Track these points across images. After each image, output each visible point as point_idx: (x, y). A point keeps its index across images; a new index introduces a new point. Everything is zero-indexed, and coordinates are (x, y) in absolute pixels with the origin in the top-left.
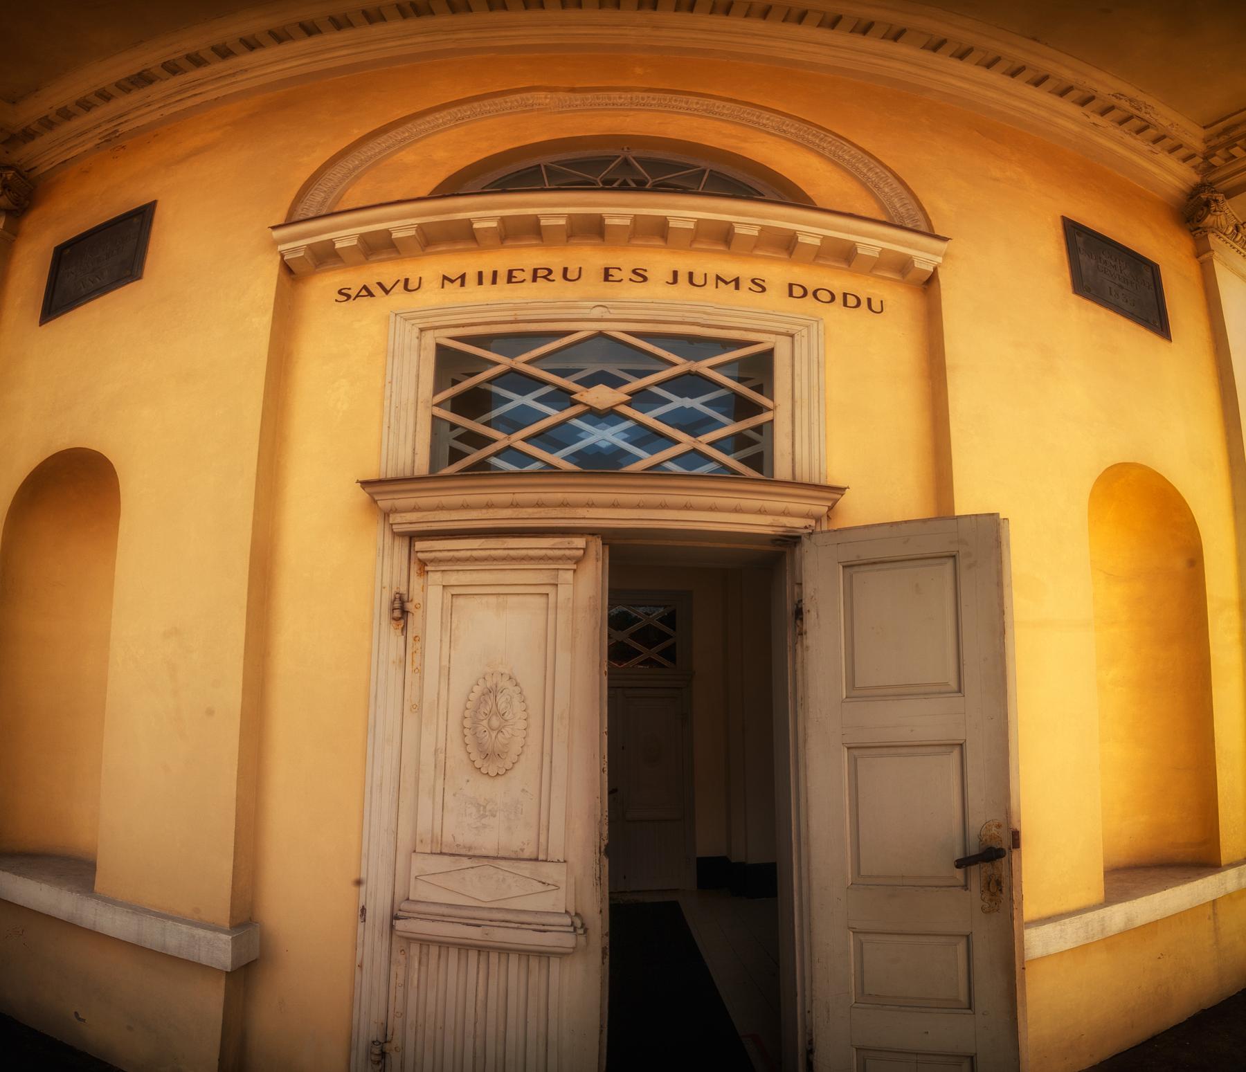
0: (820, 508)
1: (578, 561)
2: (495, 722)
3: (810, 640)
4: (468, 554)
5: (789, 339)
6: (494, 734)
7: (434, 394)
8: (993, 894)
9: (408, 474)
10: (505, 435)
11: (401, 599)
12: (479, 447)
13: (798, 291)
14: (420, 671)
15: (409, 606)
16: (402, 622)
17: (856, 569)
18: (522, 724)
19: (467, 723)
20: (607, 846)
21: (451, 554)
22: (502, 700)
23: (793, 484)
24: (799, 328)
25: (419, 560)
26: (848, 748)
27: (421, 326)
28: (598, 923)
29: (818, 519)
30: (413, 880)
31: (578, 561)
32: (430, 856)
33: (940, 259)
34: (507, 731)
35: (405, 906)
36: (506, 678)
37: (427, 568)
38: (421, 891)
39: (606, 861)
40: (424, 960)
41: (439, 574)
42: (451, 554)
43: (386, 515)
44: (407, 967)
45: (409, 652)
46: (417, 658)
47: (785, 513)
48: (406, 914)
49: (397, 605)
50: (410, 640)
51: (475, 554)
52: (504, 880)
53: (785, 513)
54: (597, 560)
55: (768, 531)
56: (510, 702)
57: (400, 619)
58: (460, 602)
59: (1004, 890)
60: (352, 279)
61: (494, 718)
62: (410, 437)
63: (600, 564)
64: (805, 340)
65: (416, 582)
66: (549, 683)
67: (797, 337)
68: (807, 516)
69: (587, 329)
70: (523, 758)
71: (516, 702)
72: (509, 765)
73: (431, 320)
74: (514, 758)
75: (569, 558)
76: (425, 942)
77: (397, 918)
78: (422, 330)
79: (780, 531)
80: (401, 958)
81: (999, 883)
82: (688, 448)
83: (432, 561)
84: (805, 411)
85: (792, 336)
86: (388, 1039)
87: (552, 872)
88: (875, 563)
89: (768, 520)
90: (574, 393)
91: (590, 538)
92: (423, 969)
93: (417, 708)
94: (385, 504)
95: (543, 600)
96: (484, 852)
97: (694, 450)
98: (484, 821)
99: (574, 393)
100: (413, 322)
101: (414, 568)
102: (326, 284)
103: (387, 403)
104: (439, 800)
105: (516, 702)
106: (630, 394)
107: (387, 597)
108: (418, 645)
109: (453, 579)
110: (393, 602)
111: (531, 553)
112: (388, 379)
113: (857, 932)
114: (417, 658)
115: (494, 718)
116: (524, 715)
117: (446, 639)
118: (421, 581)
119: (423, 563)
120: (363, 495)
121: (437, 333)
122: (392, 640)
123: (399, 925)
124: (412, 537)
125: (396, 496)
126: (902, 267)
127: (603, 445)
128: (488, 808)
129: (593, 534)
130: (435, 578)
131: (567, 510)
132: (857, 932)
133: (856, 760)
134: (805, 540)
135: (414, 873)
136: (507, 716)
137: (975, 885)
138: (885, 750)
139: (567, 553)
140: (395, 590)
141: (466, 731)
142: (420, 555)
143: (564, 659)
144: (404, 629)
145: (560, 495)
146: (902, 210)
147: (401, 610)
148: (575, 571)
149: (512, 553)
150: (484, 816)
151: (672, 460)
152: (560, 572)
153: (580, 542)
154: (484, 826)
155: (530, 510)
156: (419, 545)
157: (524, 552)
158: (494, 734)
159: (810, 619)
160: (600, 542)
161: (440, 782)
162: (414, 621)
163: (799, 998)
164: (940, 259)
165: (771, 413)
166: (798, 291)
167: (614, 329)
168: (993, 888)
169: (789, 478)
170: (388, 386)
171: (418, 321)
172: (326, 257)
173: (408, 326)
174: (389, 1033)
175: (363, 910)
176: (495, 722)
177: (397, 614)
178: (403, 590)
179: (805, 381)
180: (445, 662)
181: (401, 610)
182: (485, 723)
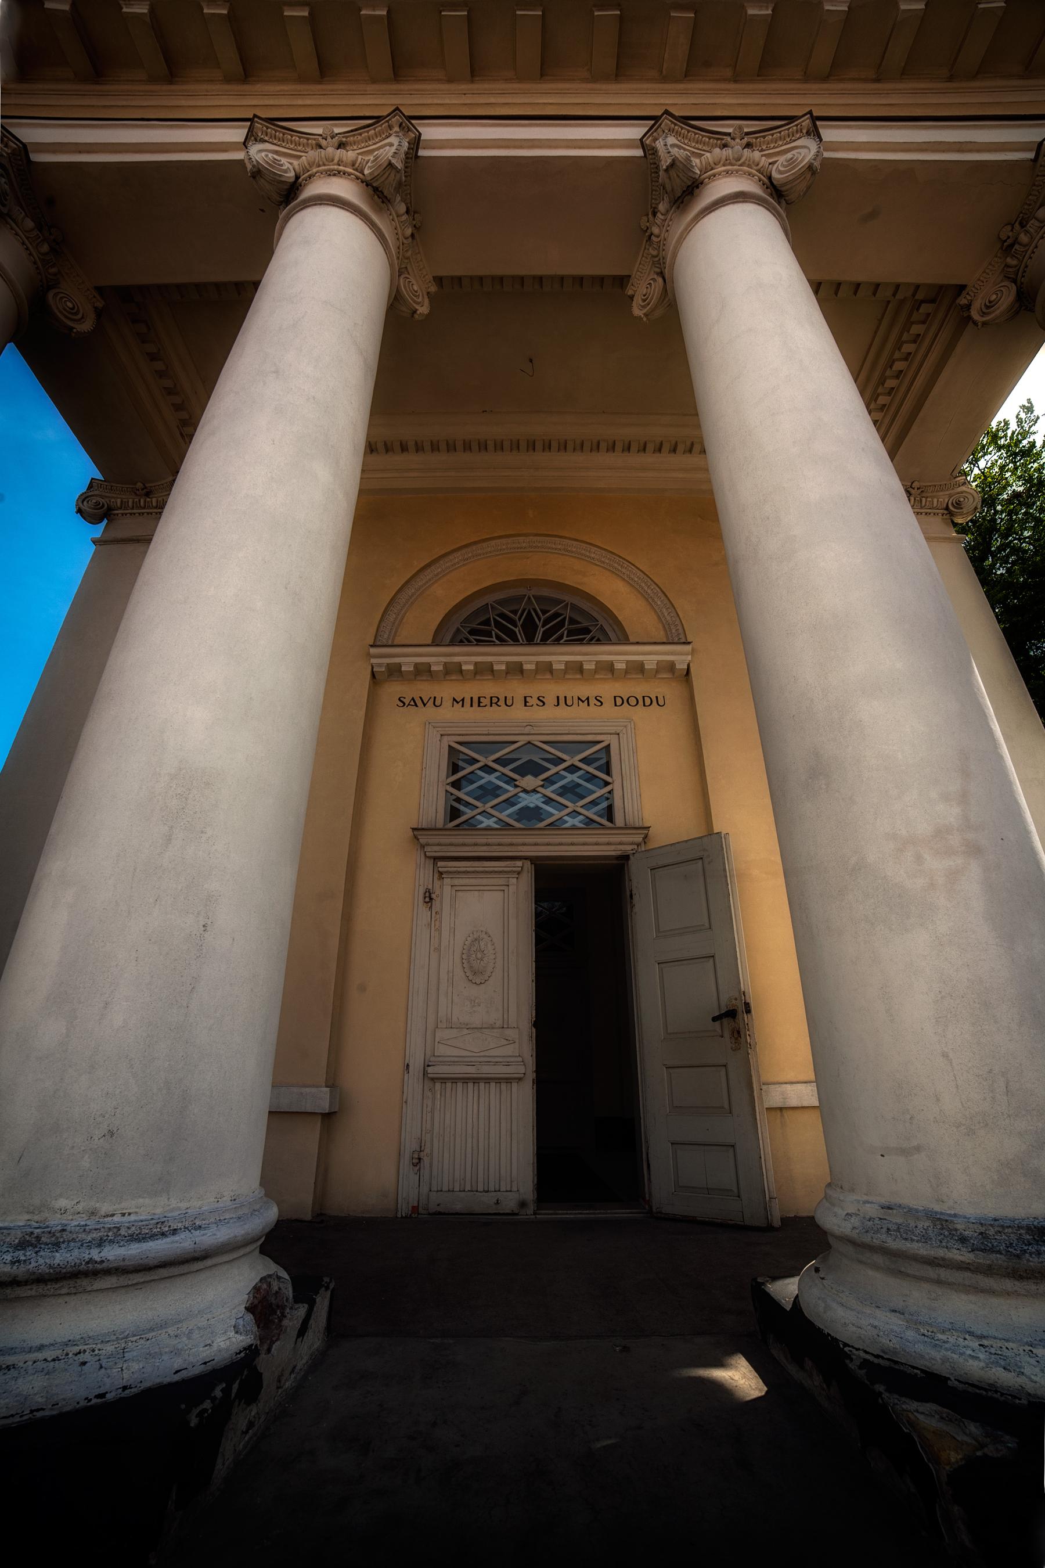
0: (639, 839)
1: (519, 873)
2: (479, 955)
3: (636, 909)
4: (465, 869)
5: (617, 736)
6: (479, 961)
7: (447, 778)
8: (736, 1039)
9: (433, 827)
10: (482, 805)
11: (429, 892)
12: (471, 765)
13: (619, 701)
14: (439, 930)
15: (433, 896)
16: (430, 904)
17: (657, 870)
18: (493, 957)
19: (464, 957)
20: (534, 1021)
21: (455, 869)
22: (482, 944)
23: (626, 828)
24: (621, 728)
25: (439, 871)
26: (659, 964)
27: (442, 733)
28: (531, 1062)
29: (638, 845)
30: (436, 1043)
31: (519, 873)
32: (446, 1030)
33: (689, 658)
34: (485, 960)
35: (433, 1059)
36: (484, 933)
37: (443, 876)
38: (442, 1050)
39: (534, 1030)
40: (443, 1094)
41: (449, 879)
42: (455, 869)
43: (423, 846)
44: (434, 1099)
45: (433, 920)
46: (437, 923)
47: (620, 844)
48: (433, 1064)
49: (427, 895)
50: (434, 913)
51: (468, 869)
52: (486, 1039)
53: (620, 844)
54: (528, 872)
55: (613, 853)
56: (486, 945)
57: (428, 902)
58: (460, 894)
59: (742, 1036)
60: (408, 691)
61: (478, 953)
62: (435, 803)
63: (530, 874)
64: (625, 736)
65: (437, 883)
66: (506, 937)
67: (621, 735)
68: (632, 844)
69: (523, 740)
70: (493, 974)
71: (489, 945)
72: (487, 978)
73: (447, 729)
74: (489, 973)
75: (514, 872)
76: (444, 1080)
77: (428, 1066)
78: (442, 735)
79: (619, 853)
80: (430, 1094)
81: (739, 1032)
82: (570, 780)
83: (446, 872)
84: (628, 782)
85: (618, 734)
86: (422, 1149)
87: (511, 1033)
88: (665, 866)
89: (613, 847)
90: (516, 781)
91: (524, 861)
92: (443, 1098)
93: (438, 950)
94: (423, 840)
95: (502, 893)
96: (474, 1026)
97: (573, 765)
98: (474, 1009)
99: (516, 781)
100: (438, 729)
101: (436, 875)
102: (394, 690)
103: (423, 781)
104: (450, 998)
105: (489, 945)
106: (542, 781)
107: (422, 891)
108: (438, 916)
109: (456, 882)
110: (425, 894)
111: (496, 869)
112: (424, 766)
113: (669, 1068)
114: (437, 923)
115: (478, 953)
116: (494, 957)
117: (453, 913)
118: (439, 882)
119: (441, 873)
120: (411, 833)
121: (450, 738)
122: (424, 914)
123: (430, 1070)
124: (436, 859)
125: (429, 837)
126: (671, 667)
127: (532, 805)
128: (476, 1001)
129: (526, 859)
130: (447, 881)
131: (513, 847)
132: (669, 1068)
133: (662, 970)
134: (631, 857)
135: (437, 1040)
136: (485, 952)
137: (727, 1034)
138: (676, 963)
139: (514, 869)
140: (426, 887)
141: (464, 961)
142: (440, 869)
143: (513, 923)
144: (431, 908)
145: (509, 840)
146: (668, 618)
147: (429, 898)
148: (517, 878)
149: (487, 869)
150: (474, 1006)
151: (564, 770)
152: (510, 879)
153: (519, 863)
154: (474, 1011)
155: (495, 847)
156: (440, 864)
157: (491, 869)
158: (479, 961)
159: (636, 898)
160: (529, 863)
161: (450, 989)
162: (436, 904)
163: (642, 1121)
164: (689, 658)
165: (611, 785)
166: (619, 701)
167: (536, 740)
168: (736, 1035)
169: (622, 825)
170: (424, 770)
171: (440, 729)
172: (394, 672)
173: (435, 733)
174: (423, 1145)
175: (408, 1065)
176: (479, 955)
177: (427, 899)
178: (430, 887)
179: (627, 763)
180: (452, 925)
181: (429, 898)
182: (474, 956)
